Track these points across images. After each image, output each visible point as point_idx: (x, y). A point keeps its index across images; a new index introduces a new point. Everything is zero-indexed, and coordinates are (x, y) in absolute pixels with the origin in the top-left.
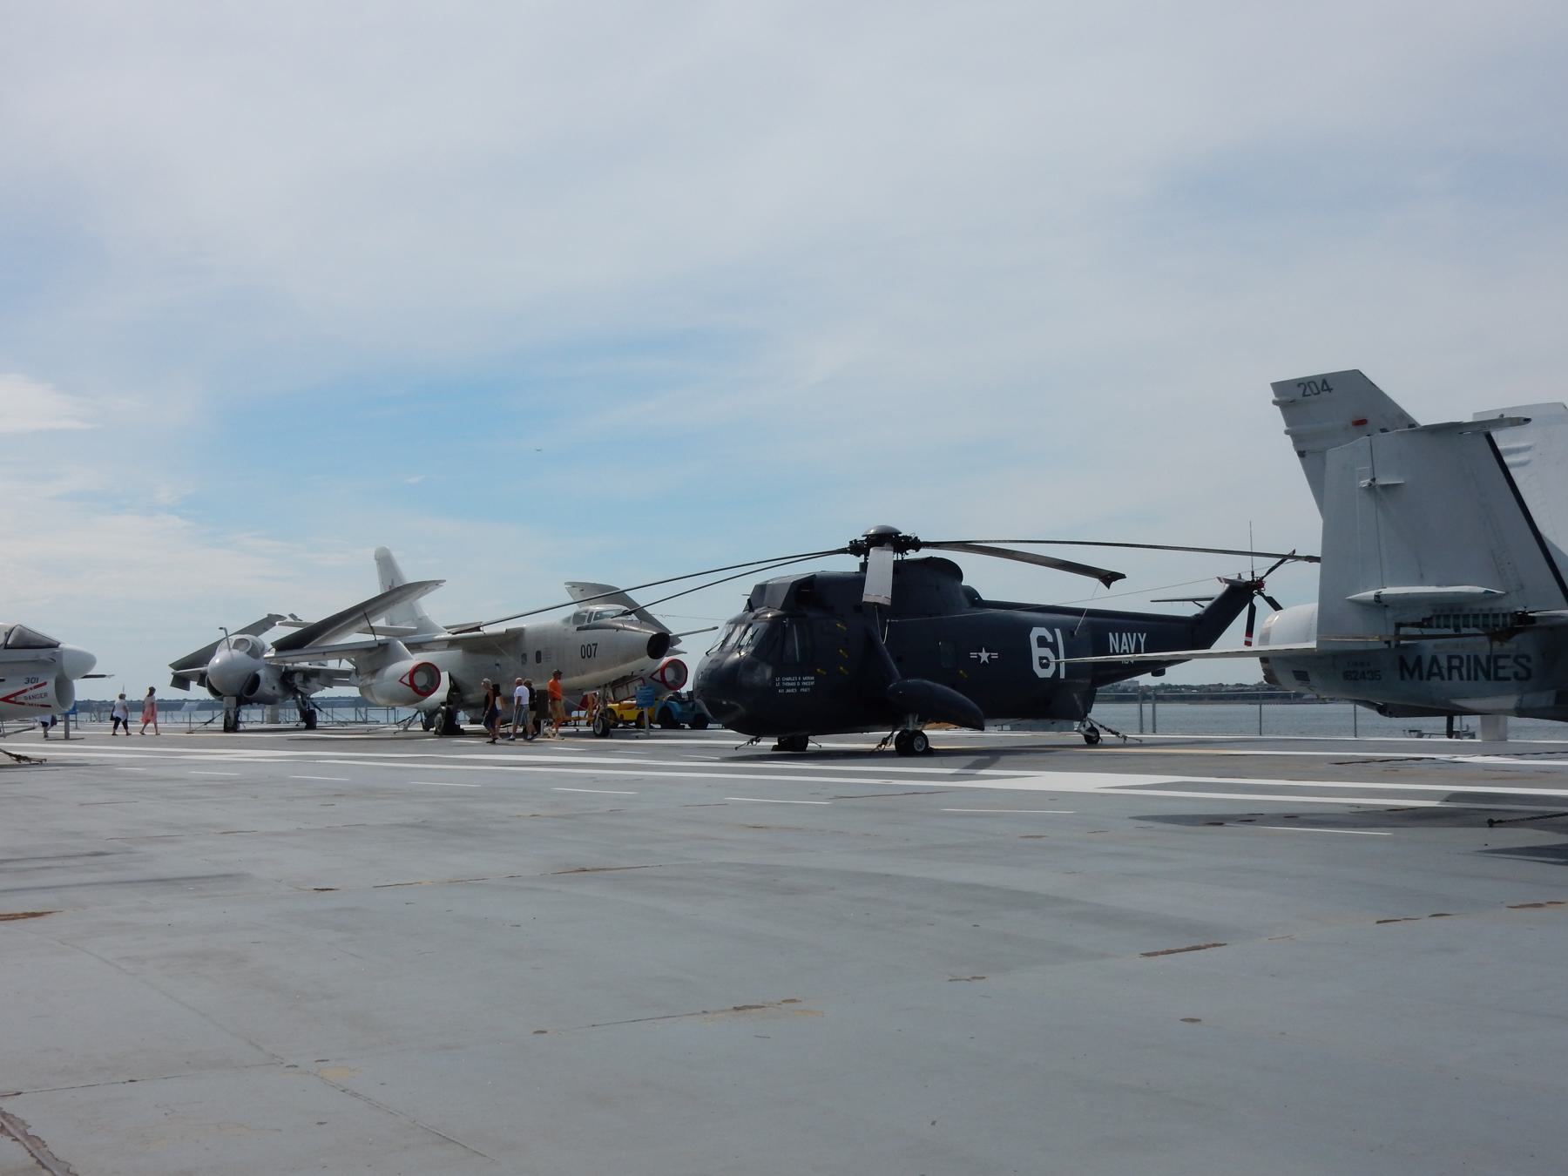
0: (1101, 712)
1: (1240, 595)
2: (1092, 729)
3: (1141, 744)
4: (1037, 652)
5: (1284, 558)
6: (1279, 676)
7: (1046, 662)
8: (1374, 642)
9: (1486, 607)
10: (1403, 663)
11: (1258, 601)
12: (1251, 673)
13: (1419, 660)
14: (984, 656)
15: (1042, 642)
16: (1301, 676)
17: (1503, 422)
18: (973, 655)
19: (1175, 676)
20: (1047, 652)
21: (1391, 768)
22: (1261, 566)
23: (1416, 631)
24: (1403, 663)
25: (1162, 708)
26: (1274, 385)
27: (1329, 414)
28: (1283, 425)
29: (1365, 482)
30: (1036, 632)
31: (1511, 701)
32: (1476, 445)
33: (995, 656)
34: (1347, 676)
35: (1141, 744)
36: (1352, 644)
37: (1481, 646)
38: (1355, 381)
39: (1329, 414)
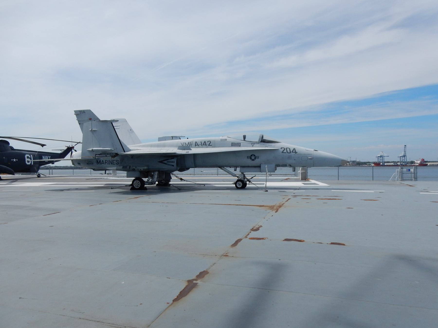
0: (40, 171)
1: (69, 150)
2: (39, 174)
3: (49, 177)
4: (27, 160)
5: (78, 143)
6: (75, 164)
7: (29, 161)
8: (92, 158)
9: (111, 152)
10: (97, 162)
11: (73, 150)
12: (69, 164)
13: (100, 161)
14: (15, 160)
15: (28, 157)
16: (79, 164)
17: (114, 121)
18: (12, 160)
19: (56, 164)
20: (29, 160)
21: (96, 180)
22: (74, 144)
23: (99, 156)
24: (97, 162)
25: (54, 170)
26: (75, 111)
27: (84, 117)
28: (76, 118)
29: (90, 129)
30: (26, 156)
31: (115, 168)
32: (110, 125)
33: (17, 160)
34: (87, 164)
35: (49, 177)
36: (87, 158)
37: (109, 158)
38: (89, 112)
39: (84, 117)
